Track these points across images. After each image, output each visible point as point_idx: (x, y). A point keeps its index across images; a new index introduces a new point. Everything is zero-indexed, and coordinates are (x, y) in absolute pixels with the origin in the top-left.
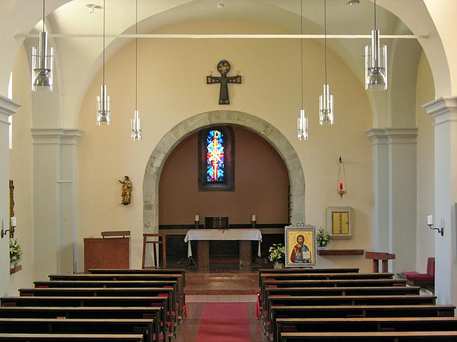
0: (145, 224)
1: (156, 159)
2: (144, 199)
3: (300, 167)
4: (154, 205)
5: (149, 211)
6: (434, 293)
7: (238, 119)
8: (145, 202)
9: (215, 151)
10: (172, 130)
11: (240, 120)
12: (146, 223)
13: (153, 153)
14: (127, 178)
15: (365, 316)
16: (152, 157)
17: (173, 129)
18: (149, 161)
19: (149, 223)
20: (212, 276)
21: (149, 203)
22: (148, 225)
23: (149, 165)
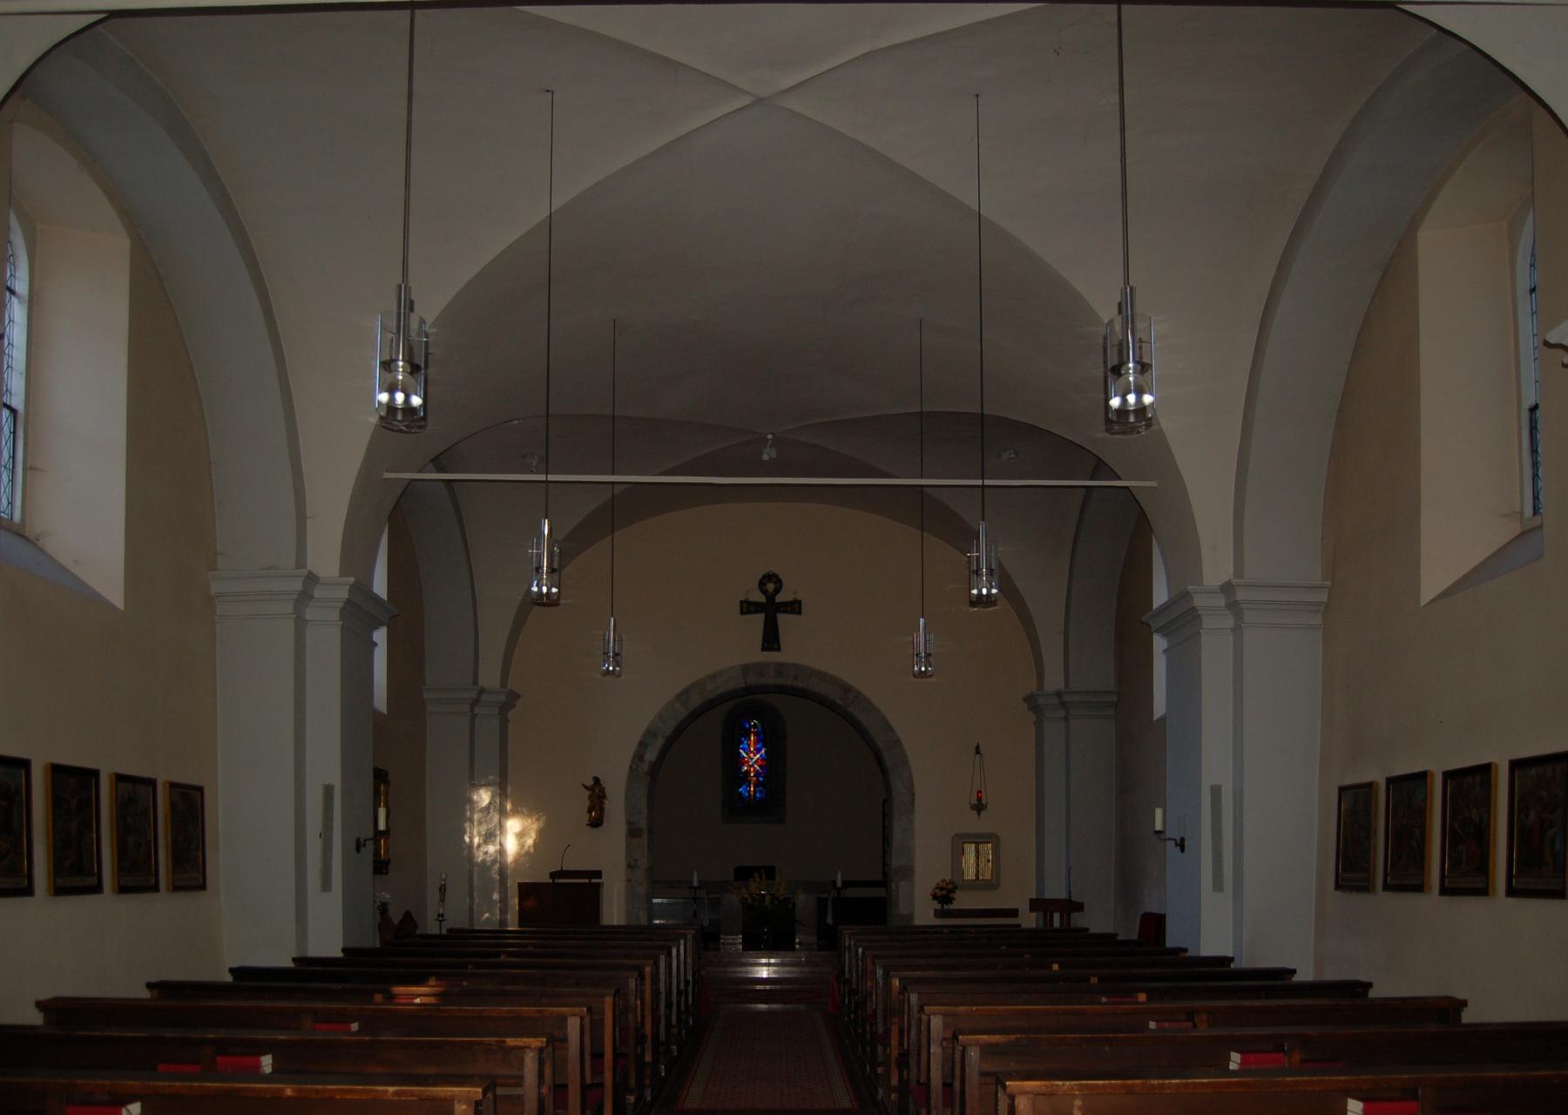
8: (629, 823)
14: (597, 780)
19: (636, 860)
22: (633, 863)
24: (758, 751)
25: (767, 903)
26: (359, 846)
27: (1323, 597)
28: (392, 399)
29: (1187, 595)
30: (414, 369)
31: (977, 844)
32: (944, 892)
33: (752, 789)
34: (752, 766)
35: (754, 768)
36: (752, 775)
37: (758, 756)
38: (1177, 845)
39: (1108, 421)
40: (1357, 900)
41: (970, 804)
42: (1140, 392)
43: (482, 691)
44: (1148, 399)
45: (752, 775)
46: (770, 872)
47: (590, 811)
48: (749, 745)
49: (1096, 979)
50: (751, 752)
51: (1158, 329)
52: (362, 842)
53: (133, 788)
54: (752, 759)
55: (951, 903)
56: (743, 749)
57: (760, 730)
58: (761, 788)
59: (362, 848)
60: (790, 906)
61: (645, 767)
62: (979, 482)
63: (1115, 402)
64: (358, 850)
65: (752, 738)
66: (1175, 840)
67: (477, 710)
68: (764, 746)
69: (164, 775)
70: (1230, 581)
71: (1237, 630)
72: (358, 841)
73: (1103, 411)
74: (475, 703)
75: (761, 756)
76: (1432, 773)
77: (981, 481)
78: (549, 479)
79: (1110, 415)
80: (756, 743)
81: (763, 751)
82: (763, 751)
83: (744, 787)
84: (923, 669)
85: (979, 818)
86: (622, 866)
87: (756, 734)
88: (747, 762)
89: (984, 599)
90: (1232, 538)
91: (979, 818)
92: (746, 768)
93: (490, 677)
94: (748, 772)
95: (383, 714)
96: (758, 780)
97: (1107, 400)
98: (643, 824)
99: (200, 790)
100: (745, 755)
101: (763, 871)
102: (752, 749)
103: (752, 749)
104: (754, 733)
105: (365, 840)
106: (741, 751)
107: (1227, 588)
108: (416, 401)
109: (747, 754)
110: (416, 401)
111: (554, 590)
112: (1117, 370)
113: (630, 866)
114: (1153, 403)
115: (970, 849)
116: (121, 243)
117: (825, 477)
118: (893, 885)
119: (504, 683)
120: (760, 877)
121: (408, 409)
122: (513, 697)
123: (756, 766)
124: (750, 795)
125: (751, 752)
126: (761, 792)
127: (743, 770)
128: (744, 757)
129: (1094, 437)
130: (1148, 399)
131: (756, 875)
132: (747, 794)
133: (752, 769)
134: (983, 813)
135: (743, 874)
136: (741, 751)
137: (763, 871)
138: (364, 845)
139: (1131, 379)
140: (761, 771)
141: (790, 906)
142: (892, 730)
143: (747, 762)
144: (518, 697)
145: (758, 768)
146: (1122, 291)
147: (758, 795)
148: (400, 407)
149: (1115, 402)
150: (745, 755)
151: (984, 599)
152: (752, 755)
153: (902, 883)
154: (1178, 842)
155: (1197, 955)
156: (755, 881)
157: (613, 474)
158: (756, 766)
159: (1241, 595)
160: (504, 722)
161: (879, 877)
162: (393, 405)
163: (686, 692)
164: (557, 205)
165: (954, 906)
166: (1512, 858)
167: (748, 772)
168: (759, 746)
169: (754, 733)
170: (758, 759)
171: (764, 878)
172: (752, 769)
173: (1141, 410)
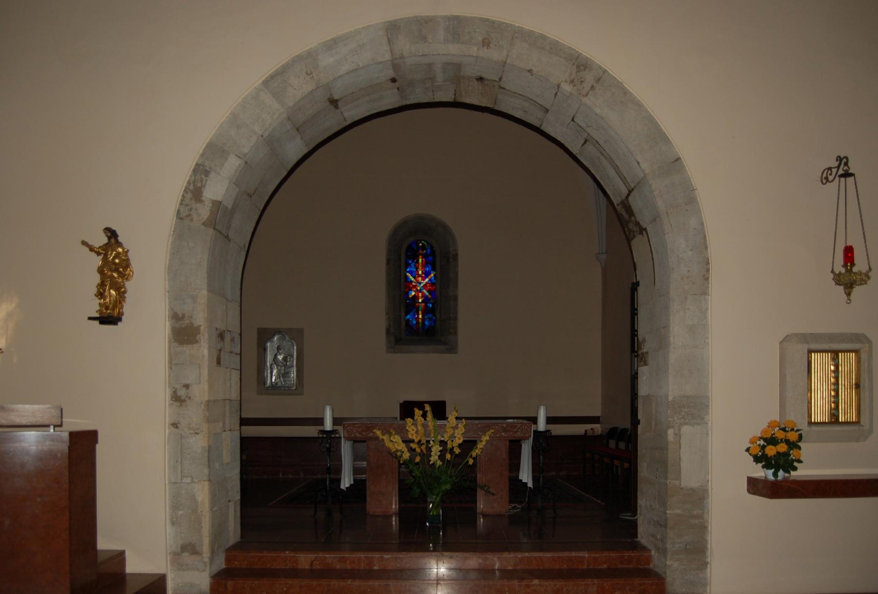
0: (175, 392)
1: (212, 175)
2: (171, 309)
3: (691, 200)
4: (202, 328)
5: (187, 350)
6: (436, 461)
7: (486, 43)
8: (175, 317)
9: (409, 254)
10: (266, 83)
11: (492, 45)
12: (177, 386)
13: (202, 155)
14: (112, 234)
15: (335, 416)
16: (201, 171)
17: (272, 77)
18: (189, 183)
19: (187, 386)
20: (395, 501)
21: (187, 322)
22: (182, 393)
23: (189, 195)
24: (427, 274)
25: (434, 458)
31: (835, 354)
32: (782, 448)
33: (420, 316)
34: (420, 291)
35: (423, 293)
36: (420, 301)
37: (427, 280)
41: (832, 271)
45: (420, 301)
46: (439, 410)
47: (101, 295)
48: (417, 268)
50: (419, 276)
54: (420, 283)
55: (795, 469)
56: (411, 272)
57: (429, 251)
58: (431, 316)
60: (471, 462)
61: (204, 212)
65: (420, 261)
68: (434, 269)
75: (430, 280)
80: (425, 265)
81: (432, 275)
82: (432, 275)
83: (411, 313)
85: (849, 301)
86: (161, 394)
87: (425, 256)
88: (415, 287)
91: (849, 301)
92: (413, 293)
94: (415, 298)
95: (417, 407)
96: (426, 306)
98: (200, 319)
100: (413, 279)
101: (428, 408)
102: (420, 272)
103: (420, 272)
104: (422, 255)
106: (408, 274)
109: (414, 278)
113: (176, 398)
115: (821, 363)
118: (671, 432)
120: (424, 416)
123: (424, 291)
124: (418, 322)
125: (419, 276)
126: (430, 319)
127: (410, 296)
128: (412, 282)
131: (418, 413)
132: (414, 322)
133: (420, 295)
134: (857, 290)
135: (408, 409)
136: (408, 274)
137: (428, 408)
140: (430, 296)
141: (471, 462)
142: (666, 140)
143: (415, 287)
145: (427, 294)
147: (427, 323)
150: (413, 279)
152: (420, 279)
153: (686, 429)
156: (415, 424)
158: (424, 291)
161: (59, 423)
163: (281, 73)
165: (802, 472)
167: (415, 298)
168: (427, 269)
169: (422, 255)
170: (427, 283)
171: (430, 415)
172: (420, 295)
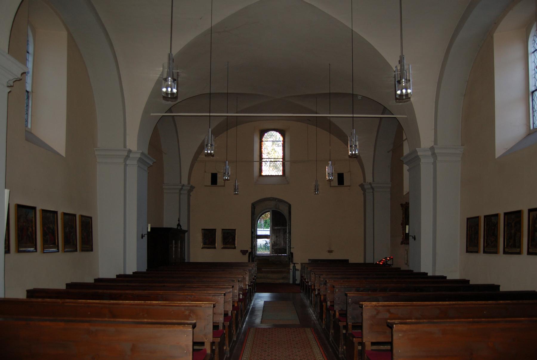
26: (142, 237)
27: (151, 163)
28: (167, 90)
29: (416, 152)
30: (174, 80)
38: (413, 238)
39: (396, 99)
40: (473, 256)
42: (406, 89)
43: (183, 185)
44: (409, 91)
49: (360, 349)
51: (412, 72)
52: (144, 235)
53: (69, 218)
59: (144, 237)
62: (352, 115)
63: (399, 92)
64: (142, 238)
66: (412, 236)
67: (182, 192)
69: (78, 213)
70: (433, 146)
71: (434, 164)
72: (142, 235)
73: (394, 95)
74: (181, 189)
76: (500, 214)
77: (352, 115)
78: (211, 115)
79: (397, 97)
84: (330, 178)
89: (209, 154)
90: (433, 136)
93: (185, 181)
97: (396, 92)
99: (91, 218)
105: (145, 235)
107: (432, 148)
108: (175, 91)
110: (175, 91)
111: (212, 152)
112: (399, 82)
114: (411, 92)
116: (65, 34)
117: (299, 114)
119: (189, 183)
121: (172, 93)
122: (192, 188)
129: (391, 104)
130: (409, 91)
138: (144, 236)
139: (404, 85)
144: (194, 188)
146: (400, 56)
148: (169, 93)
149: (399, 92)
151: (354, 155)
154: (413, 237)
155: (420, 272)
157: (227, 113)
159: (373, 185)
160: (189, 195)
162: (168, 93)
164: (213, 24)
166: (505, 224)
173: (407, 94)
